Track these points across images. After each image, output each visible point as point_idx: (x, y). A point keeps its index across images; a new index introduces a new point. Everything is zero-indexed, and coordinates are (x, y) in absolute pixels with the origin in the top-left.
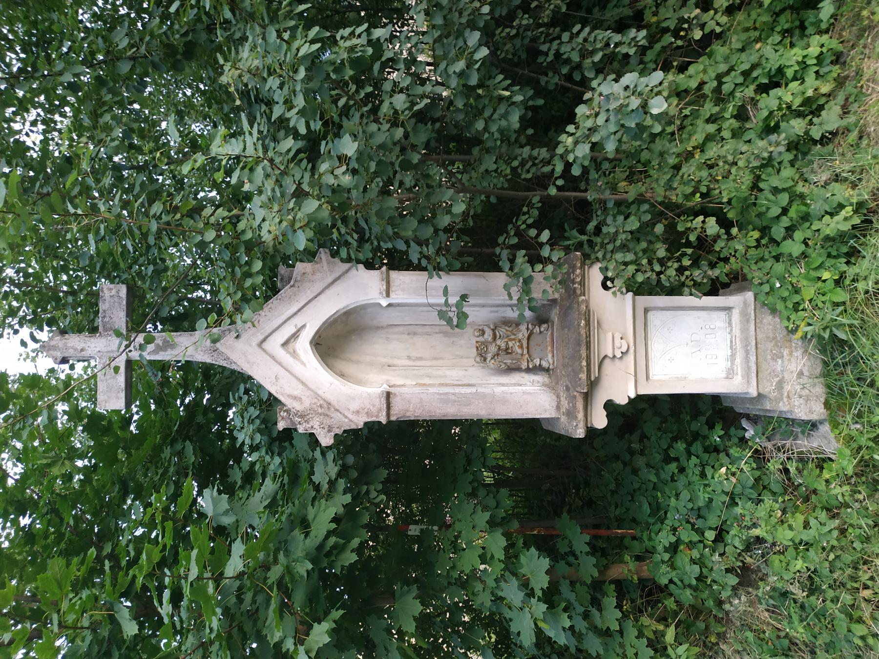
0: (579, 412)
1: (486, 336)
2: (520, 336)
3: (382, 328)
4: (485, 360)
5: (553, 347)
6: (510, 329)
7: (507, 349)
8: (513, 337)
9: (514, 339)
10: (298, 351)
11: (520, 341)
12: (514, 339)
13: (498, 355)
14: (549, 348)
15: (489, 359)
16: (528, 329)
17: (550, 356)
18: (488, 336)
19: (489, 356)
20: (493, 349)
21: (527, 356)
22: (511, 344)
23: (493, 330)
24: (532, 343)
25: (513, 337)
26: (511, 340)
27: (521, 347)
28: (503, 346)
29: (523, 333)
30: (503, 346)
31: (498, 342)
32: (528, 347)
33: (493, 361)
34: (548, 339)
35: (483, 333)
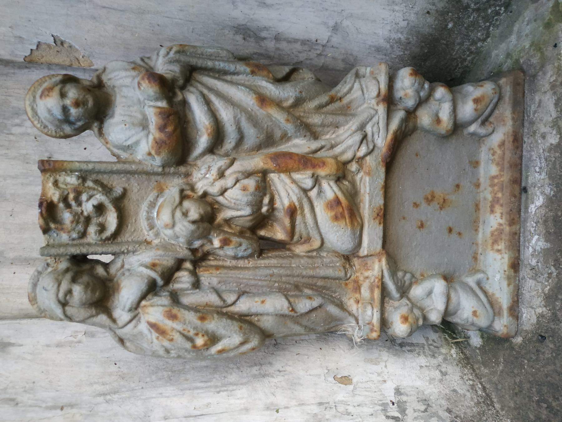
0: (177, 324)
1: (118, 129)
2: (345, 140)
3: (143, 297)
4: (101, 297)
5: (516, 216)
6: (287, 93)
7: (261, 220)
8: (300, 145)
9: (306, 161)
10: (38, 286)
11: (341, 175)
12: (306, 161)
13: (199, 258)
14: (494, 220)
15: (128, 292)
16: (389, 100)
17: (496, 263)
18: (133, 127)
19: (133, 272)
20: (162, 223)
21: (378, 267)
22: (285, 190)
23: (167, 88)
24: (408, 189)
25: (300, 145)
26: (288, 163)
27: (348, 209)
28: (237, 203)
29: (360, 127)
30: (237, 203)
31: (205, 175)
32: (384, 215)
33: (155, 311)
34: (489, 169)
35: (95, 106)
